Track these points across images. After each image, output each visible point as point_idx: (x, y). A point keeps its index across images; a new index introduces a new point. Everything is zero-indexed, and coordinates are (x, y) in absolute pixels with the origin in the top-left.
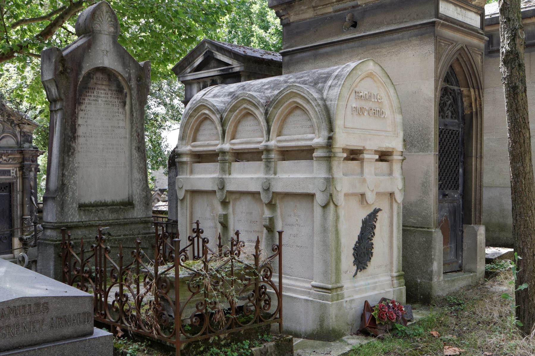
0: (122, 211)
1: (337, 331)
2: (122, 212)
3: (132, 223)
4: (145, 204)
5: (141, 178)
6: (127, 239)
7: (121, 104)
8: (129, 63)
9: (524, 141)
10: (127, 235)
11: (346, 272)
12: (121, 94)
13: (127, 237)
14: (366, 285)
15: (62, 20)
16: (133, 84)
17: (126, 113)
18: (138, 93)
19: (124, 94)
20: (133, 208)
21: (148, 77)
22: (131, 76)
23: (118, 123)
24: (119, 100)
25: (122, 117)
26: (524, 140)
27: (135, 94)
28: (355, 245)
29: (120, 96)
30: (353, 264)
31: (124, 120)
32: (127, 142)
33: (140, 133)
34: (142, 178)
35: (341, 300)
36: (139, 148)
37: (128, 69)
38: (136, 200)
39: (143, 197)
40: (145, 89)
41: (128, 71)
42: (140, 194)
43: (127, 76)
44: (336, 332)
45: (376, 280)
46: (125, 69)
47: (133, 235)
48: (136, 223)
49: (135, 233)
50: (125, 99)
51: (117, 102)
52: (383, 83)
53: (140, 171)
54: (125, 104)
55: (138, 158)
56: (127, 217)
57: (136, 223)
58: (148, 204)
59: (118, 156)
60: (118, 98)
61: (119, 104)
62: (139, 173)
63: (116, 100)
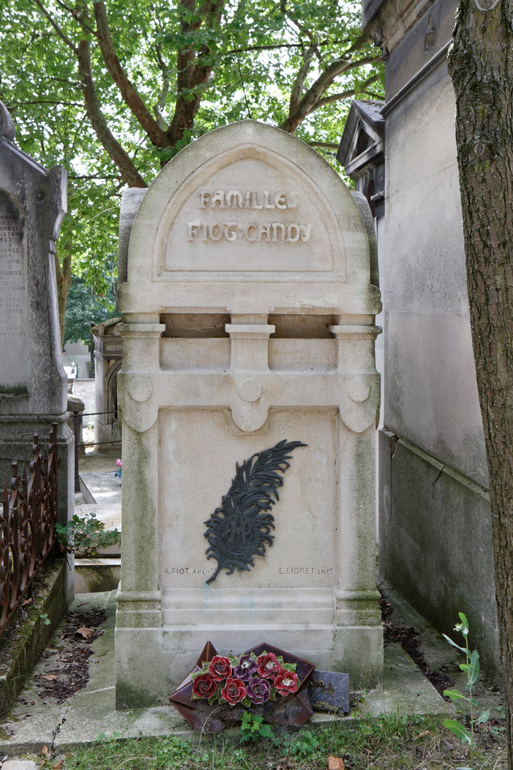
0: (7, 402)
1: (134, 689)
2: (7, 405)
3: (23, 422)
4: (49, 392)
5: (41, 351)
6: (10, 446)
7: (16, 236)
8: (23, 173)
9: (487, 300)
10: (12, 440)
11: (183, 571)
12: (15, 222)
13: (9, 443)
14: (242, 605)
15: (313, 94)
16: (29, 204)
17: (23, 249)
18: (37, 218)
19: (20, 221)
20: (27, 398)
21: (55, 191)
22: (25, 194)
23: (10, 266)
24: (12, 231)
25: (16, 256)
26: (487, 295)
27: (32, 220)
28: (213, 516)
29: (13, 225)
30: (206, 556)
31: (20, 261)
32: (26, 295)
33: (40, 280)
34: (44, 351)
35: (149, 629)
36: (38, 304)
37: (20, 183)
38: (33, 387)
39: (45, 382)
40: (51, 211)
41: (21, 185)
42: (38, 377)
43: (19, 193)
44: (131, 692)
45: (284, 599)
46: (14, 183)
47: (21, 441)
48: (32, 422)
49: (26, 438)
50: (22, 228)
51: (7, 234)
52: (293, 166)
53: (40, 341)
54: (21, 236)
55: (36, 320)
56: (14, 411)
57: (32, 422)
58: (54, 394)
59: (9, 317)
60: (9, 228)
61: (12, 237)
62: (38, 343)
63: (6, 232)
